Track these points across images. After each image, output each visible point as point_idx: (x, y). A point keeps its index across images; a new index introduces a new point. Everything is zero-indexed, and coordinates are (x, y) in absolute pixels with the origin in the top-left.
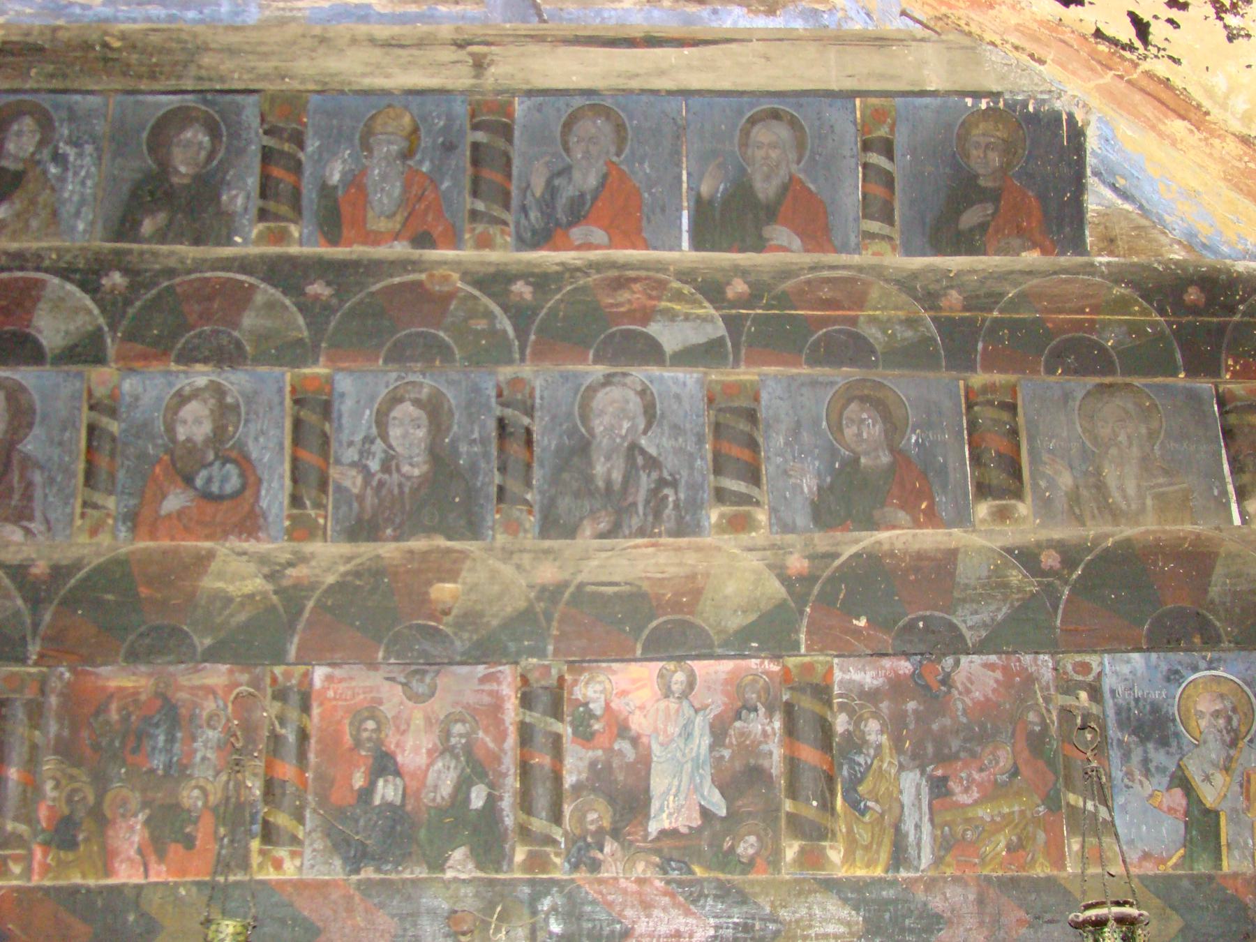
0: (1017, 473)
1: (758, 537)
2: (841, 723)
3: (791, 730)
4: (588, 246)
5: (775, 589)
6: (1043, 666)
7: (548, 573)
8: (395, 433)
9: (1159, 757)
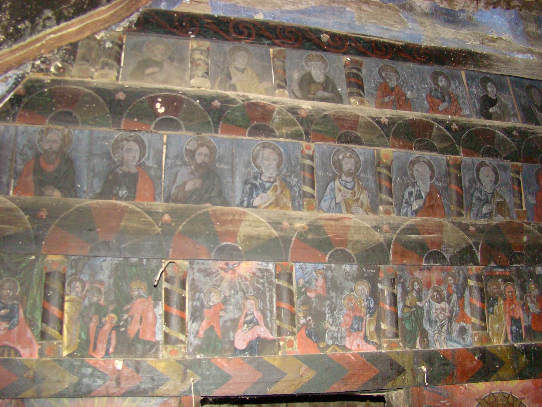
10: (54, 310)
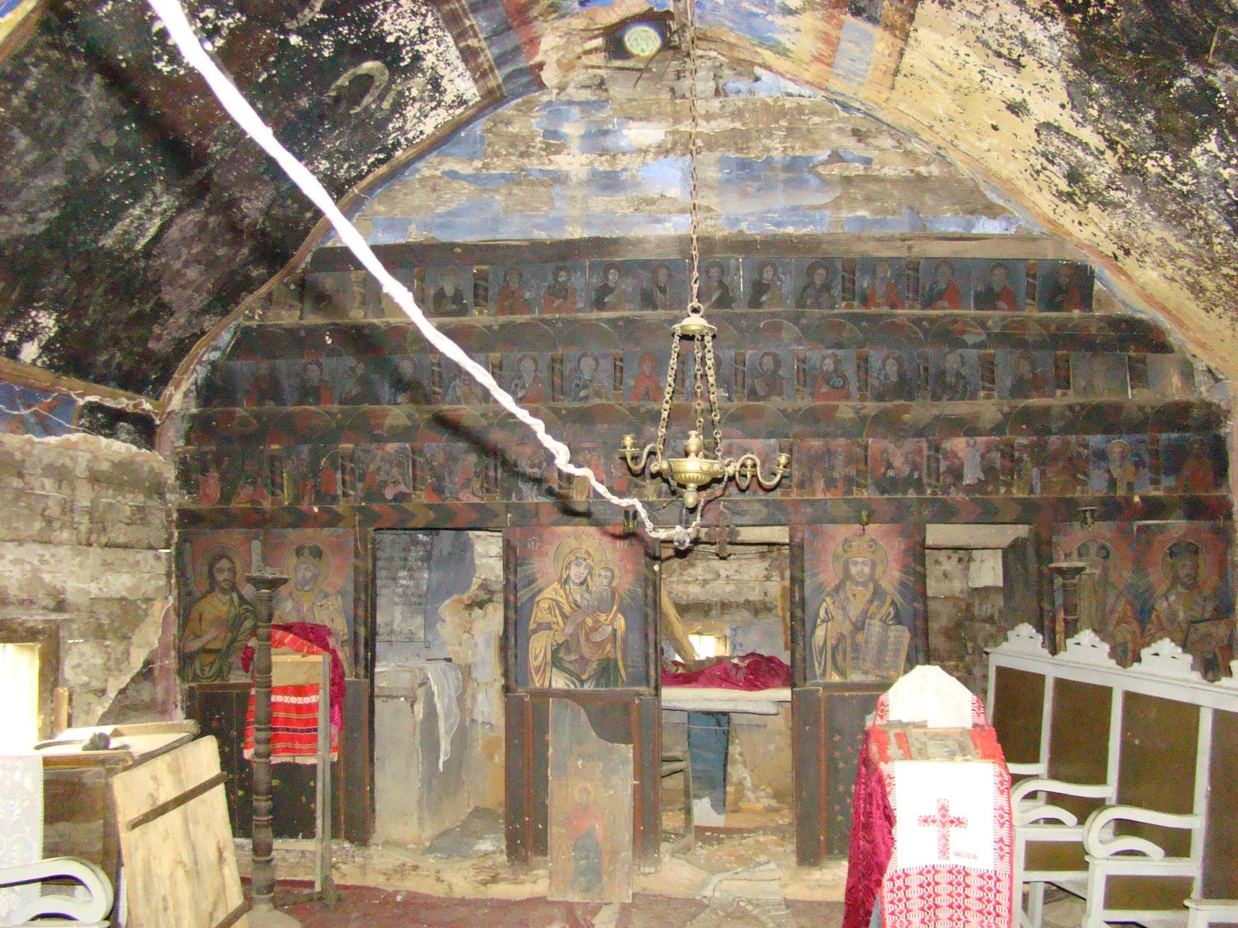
0: (1068, 382)
1: (994, 401)
2: (1017, 454)
3: (1003, 456)
4: (943, 308)
5: (1000, 416)
6: (1073, 438)
7: (935, 412)
8: (887, 368)
9: (1103, 464)
10: (278, 480)
